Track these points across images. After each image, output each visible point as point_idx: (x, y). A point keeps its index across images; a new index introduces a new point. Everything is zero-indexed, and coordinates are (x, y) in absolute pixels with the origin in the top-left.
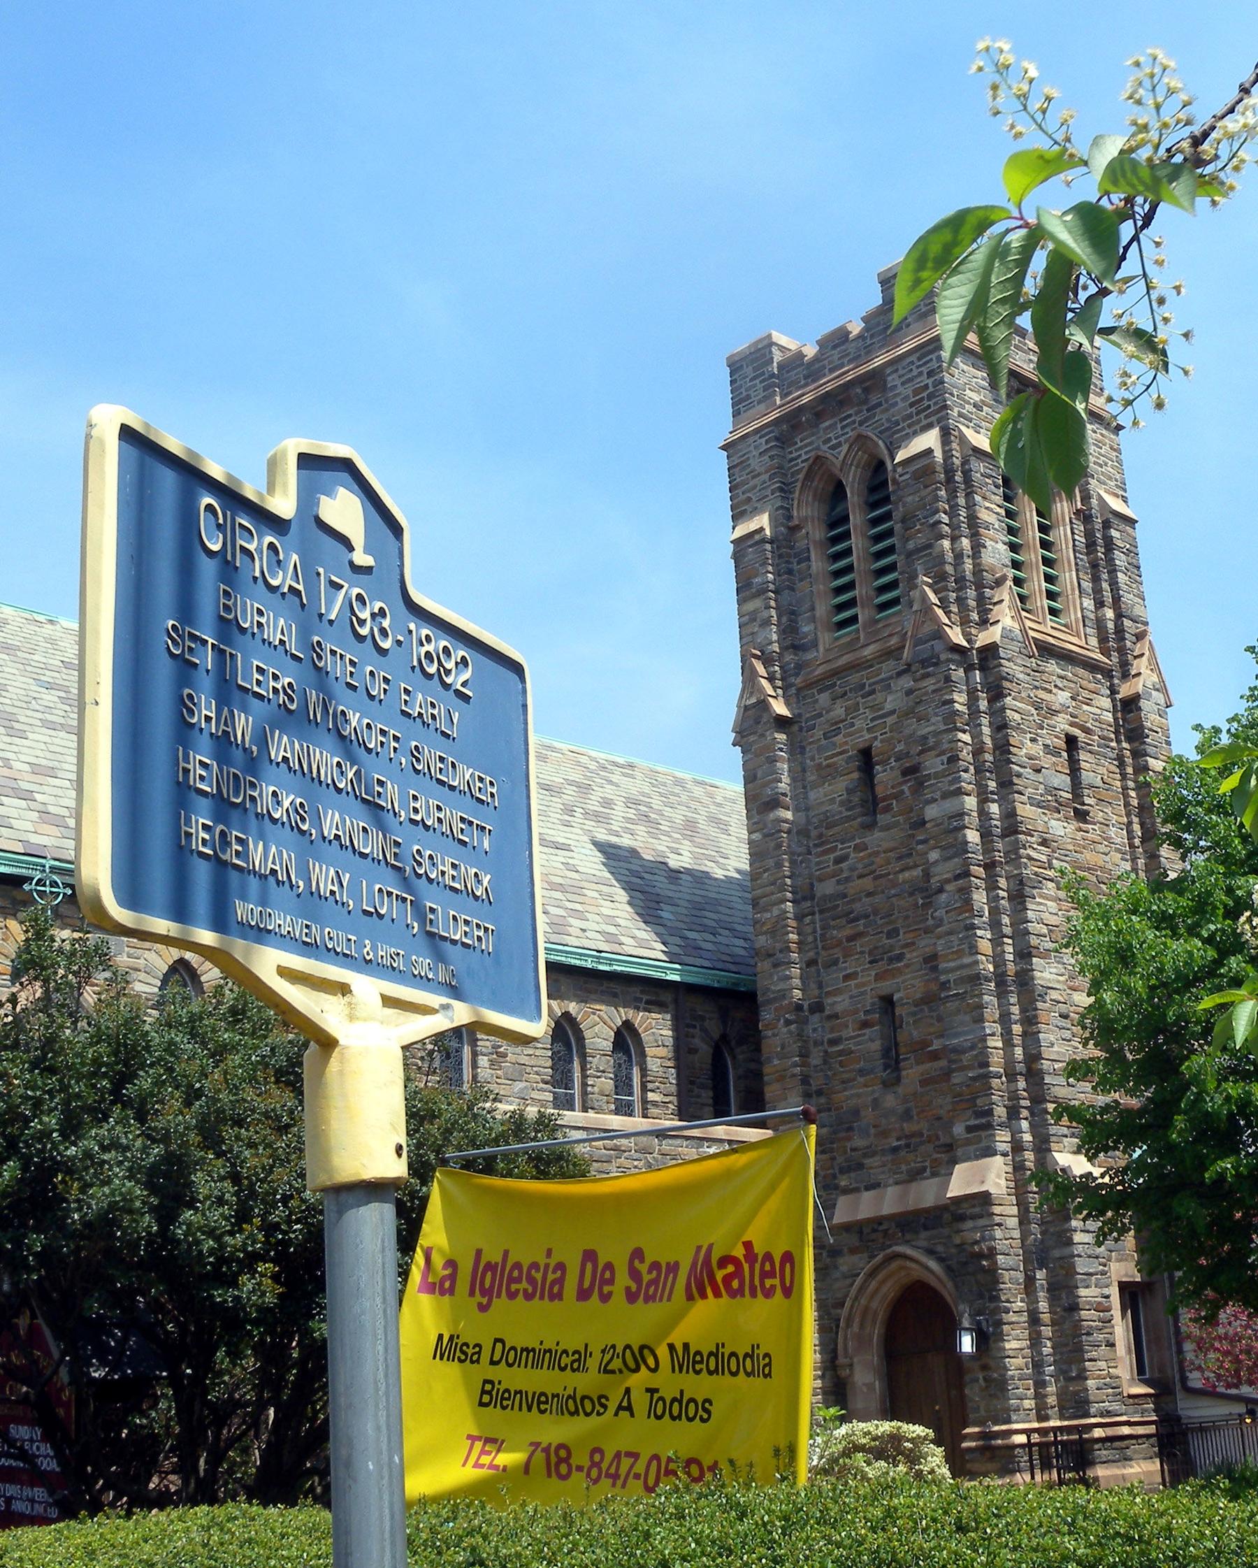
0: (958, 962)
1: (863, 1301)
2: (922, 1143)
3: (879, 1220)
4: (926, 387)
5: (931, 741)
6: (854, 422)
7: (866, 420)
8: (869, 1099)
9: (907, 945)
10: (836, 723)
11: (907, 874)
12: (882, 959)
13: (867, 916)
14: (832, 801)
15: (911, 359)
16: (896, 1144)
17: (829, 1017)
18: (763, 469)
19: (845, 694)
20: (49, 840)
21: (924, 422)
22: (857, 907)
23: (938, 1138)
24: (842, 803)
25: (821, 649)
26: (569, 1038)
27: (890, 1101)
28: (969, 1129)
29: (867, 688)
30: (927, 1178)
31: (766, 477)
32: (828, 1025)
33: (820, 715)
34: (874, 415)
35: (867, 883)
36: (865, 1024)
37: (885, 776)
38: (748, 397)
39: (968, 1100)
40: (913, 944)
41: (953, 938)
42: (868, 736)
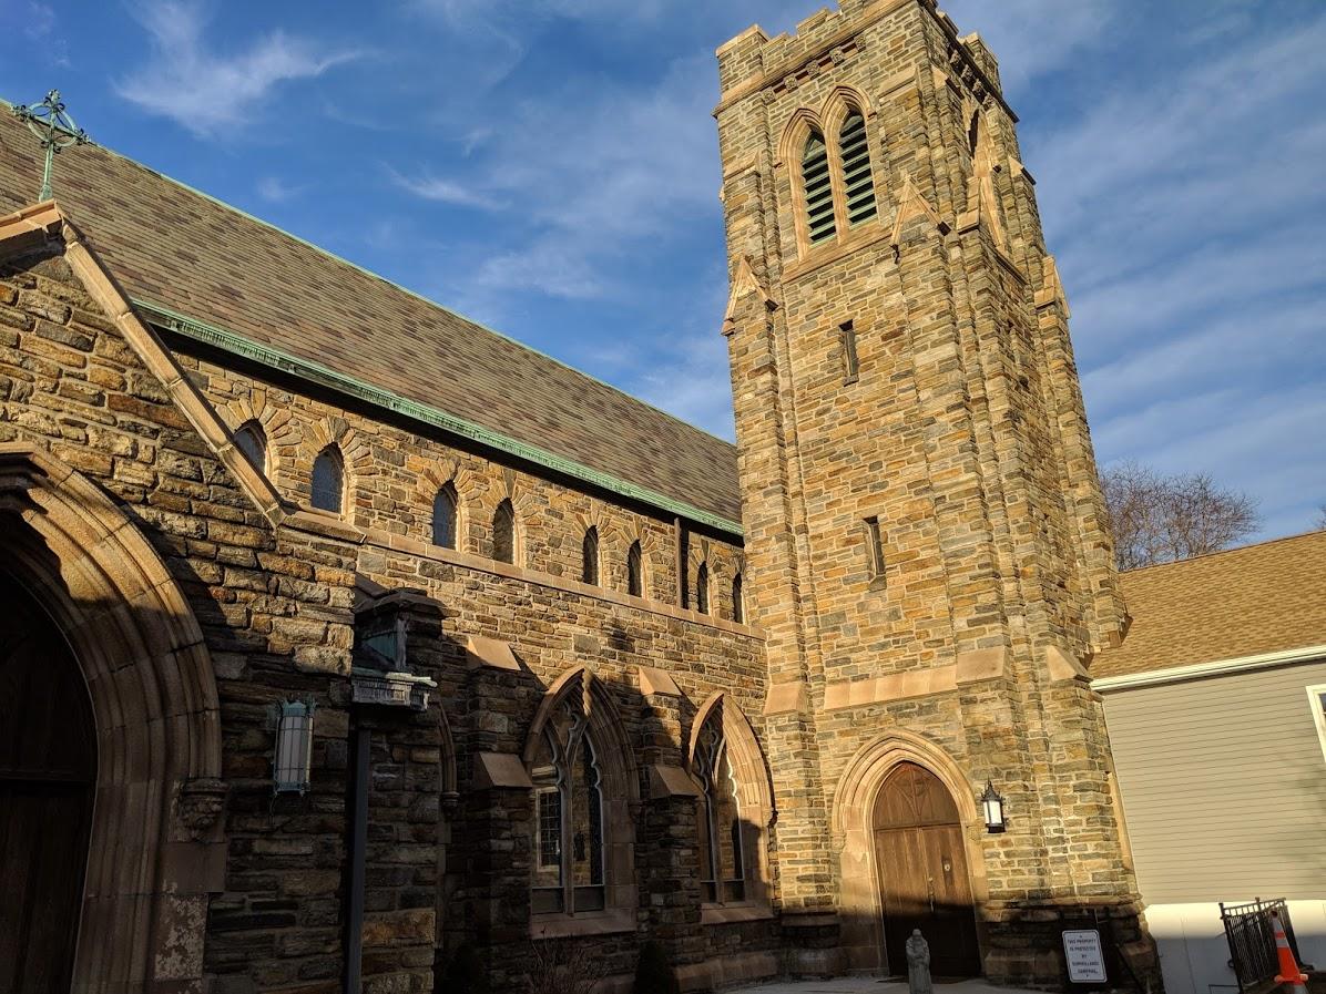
1: (855, 779)
3: (871, 706)
4: (904, 36)
6: (832, 80)
8: (855, 603)
10: (819, 306)
12: (866, 487)
13: (849, 454)
14: (815, 367)
15: (888, 18)
16: (883, 640)
17: (813, 538)
18: (750, 124)
19: (826, 283)
21: (902, 64)
22: (840, 449)
24: (823, 368)
27: (877, 604)
28: (971, 623)
29: (847, 276)
30: (917, 669)
31: (753, 130)
34: (851, 71)
35: (851, 428)
36: (849, 542)
37: (866, 344)
38: (736, 75)
40: (897, 473)
42: (848, 313)
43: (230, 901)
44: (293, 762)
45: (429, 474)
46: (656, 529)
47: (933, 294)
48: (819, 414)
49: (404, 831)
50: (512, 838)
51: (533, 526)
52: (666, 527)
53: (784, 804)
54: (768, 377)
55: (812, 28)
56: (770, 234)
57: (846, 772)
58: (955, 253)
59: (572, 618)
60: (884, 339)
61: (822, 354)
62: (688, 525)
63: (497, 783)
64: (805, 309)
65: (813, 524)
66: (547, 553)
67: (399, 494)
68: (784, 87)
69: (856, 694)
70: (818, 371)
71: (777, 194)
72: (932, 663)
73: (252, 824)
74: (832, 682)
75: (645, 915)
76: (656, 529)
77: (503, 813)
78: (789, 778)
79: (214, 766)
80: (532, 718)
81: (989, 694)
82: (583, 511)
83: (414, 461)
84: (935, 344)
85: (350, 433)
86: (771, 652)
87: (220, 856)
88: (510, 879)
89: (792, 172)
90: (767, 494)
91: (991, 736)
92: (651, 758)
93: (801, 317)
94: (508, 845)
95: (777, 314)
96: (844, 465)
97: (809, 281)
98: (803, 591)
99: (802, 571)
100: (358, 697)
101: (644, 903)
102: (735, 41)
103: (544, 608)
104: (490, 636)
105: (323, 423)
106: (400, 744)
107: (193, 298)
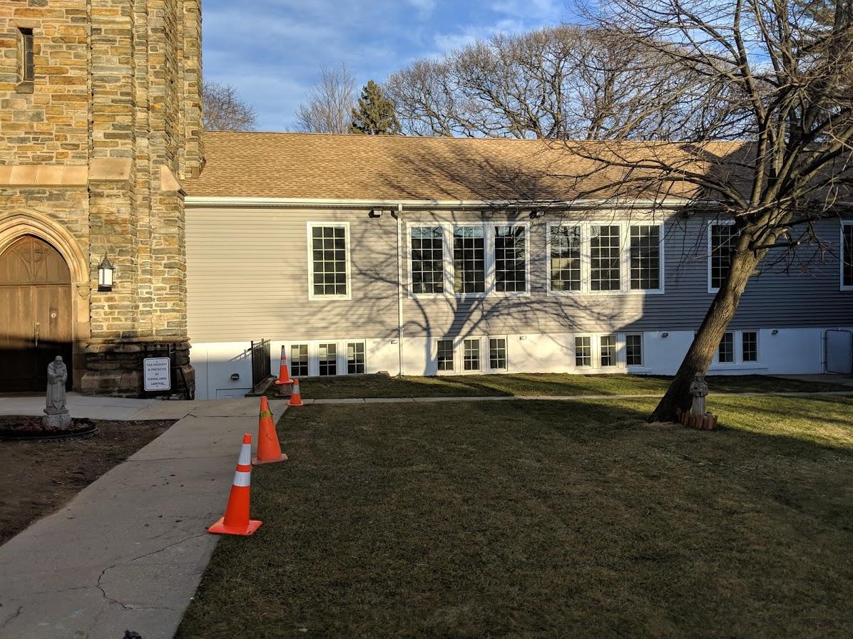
0: (112, 19)
2: (51, 139)
16: (23, 135)
20: (641, 299)
23: (66, 139)
26: (845, 273)
27: (21, 104)
28: (107, 136)
30: (53, 164)
39: (109, 116)
72: (67, 161)
81: (115, 192)
91: (111, 223)
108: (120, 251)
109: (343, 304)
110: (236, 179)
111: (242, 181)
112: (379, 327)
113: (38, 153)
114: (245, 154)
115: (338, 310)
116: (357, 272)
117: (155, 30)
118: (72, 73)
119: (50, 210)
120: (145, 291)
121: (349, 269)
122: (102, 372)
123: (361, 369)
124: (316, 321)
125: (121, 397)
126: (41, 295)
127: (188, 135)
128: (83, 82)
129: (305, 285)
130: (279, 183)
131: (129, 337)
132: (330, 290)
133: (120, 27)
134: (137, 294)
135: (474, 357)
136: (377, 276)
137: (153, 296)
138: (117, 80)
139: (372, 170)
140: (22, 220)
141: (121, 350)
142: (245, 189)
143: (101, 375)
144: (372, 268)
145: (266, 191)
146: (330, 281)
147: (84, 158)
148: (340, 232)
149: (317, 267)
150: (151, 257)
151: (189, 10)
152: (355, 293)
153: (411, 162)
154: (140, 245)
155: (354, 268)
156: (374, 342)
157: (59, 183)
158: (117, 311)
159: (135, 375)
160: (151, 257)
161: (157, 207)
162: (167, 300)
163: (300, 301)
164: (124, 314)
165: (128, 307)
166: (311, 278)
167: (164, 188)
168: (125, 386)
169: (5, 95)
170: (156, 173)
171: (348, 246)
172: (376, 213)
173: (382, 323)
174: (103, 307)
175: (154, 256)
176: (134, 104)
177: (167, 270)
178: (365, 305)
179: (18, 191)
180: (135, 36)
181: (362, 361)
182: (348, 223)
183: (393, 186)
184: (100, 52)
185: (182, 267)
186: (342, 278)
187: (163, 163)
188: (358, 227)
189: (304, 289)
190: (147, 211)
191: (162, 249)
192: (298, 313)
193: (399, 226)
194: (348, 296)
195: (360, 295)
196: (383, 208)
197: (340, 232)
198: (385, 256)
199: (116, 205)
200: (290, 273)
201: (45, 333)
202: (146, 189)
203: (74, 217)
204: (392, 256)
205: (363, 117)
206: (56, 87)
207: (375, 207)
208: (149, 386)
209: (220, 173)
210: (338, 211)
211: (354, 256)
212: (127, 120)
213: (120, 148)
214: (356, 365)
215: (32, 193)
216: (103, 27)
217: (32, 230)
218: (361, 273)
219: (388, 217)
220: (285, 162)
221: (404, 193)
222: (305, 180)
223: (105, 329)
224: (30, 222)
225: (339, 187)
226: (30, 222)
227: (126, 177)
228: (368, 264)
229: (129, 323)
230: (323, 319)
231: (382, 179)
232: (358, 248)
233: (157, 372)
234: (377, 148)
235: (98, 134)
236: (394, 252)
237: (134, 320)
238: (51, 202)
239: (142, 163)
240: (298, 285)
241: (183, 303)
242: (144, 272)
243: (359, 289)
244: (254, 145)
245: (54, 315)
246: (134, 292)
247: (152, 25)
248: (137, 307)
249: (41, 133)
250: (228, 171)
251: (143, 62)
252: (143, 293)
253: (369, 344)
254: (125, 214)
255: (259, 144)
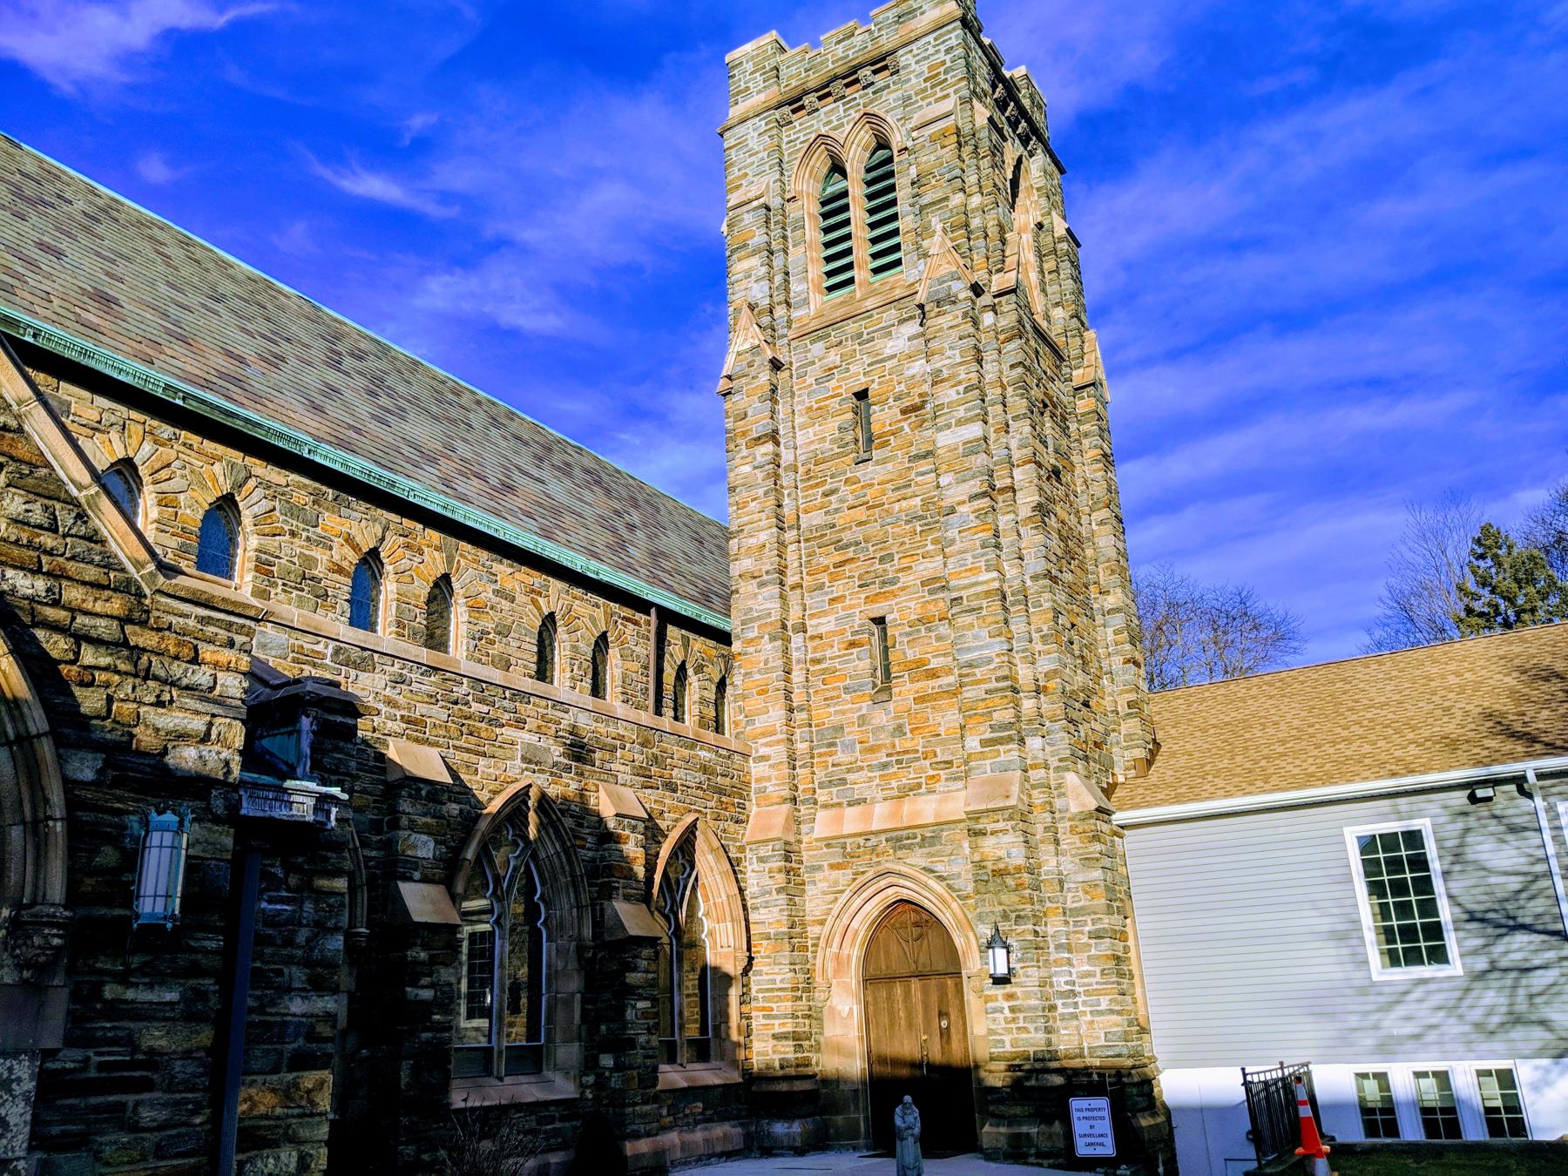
0: (973, 580)
2: (918, 759)
4: (944, 63)
5: (945, 374)
7: (872, 102)
9: (902, 570)
11: (904, 504)
13: (858, 544)
16: (885, 759)
17: (812, 638)
21: (939, 95)
22: (847, 537)
24: (833, 441)
25: (812, 306)
27: (881, 717)
28: (985, 743)
32: (810, 644)
33: (813, 363)
36: (852, 644)
37: (883, 417)
39: (983, 715)
41: (969, 556)
42: (863, 379)
43: (69, 1060)
44: (159, 885)
45: (349, 540)
46: (628, 620)
47: (961, 364)
48: (826, 495)
49: (298, 975)
50: (432, 986)
51: (476, 609)
52: (640, 617)
53: (762, 949)
54: (769, 447)
55: (839, 42)
56: (778, 279)
57: (835, 912)
58: (988, 319)
59: (520, 723)
60: (904, 412)
61: (832, 425)
62: (667, 617)
63: (416, 918)
64: (815, 372)
65: (815, 622)
66: (492, 643)
67: (310, 562)
68: (802, 107)
69: (852, 820)
70: (827, 445)
71: (789, 233)
72: (940, 787)
73: (103, 964)
74: (825, 806)
75: (591, 1079)
76: (628, 620)
77: (423, 955)
78: (770, 917)
79: (56, 888)
80: (464, 843)
81: (1001, 825)
82: (540, 594)
83: (331, 522)
84: (960, 423)
85: (252, 483)
86: (756, 770)
87: (58, 1005)
88: (426, 1035)
89: (808, 210)
90: (762, 585)
91: (1000, 873)
92: (607, 892)
93: (810, 380)
94: (427, 994)
95: (783, 375)
96: (851, 555)
97: (820, 338)
98: (797, 700)
99: (797, 676)
100: (248, 809)
101: (589, 1064)
102: (748, 48)
103: (485, 709)
104: (417, 740)
105: (217, 468)
106: (298, 869)
107: (56, 302)
108: (1018, 917)
109: (1445, 985)
110: (1208, 768)
111: (1219, 771)
112: (1538, 1033)
113: (904, 781)
114: (1227, 719)
115: (1437, 999)
116: (1465, 916)
117: (1035, 578)
118: (935, 663)
119: (924, 863)
120: (1062, 980)
121: (1445, 913)
122: (1012, 1121)
123: (1519, 1127)
124: (1393, 1023)
125: (1040, 1165)
126: (925, 992)
127: (1123, 709)
128: (950, 671)
129: (1360, 950)
130: (1283, 764)
131: (1043, 1060)
132: (1413, 957)
133: (986, 588)
134: (1052, 985)
135: (1508, 1110)
136: (1511, 923)
137: (1077, 988)
138: (990, 661)
139: (1468, 708)
140: (883, 883)
141: (1033, 1083)
142: (1221, 783)
143: (1009, 1125)
144: (1496, 906)
145: (1259, 784)
146: (1414, 939)
147: (960, 778)
148: (1414, 838)
149: (1384, 912)
150: (1067, 922)
151: (1101, 523)
152: (1469, 960)
153: (1558, 676)
154: (1048, 904)
155: (1457, 910)
156: (1537, 1068)
157: (931, 820)
158: (1021, 1016)
159: (1057, 1127)
160: (1067, 922)
161: (1069, 841)
162: (1098, 993)
163: (1356, 983)
164: (1032, 1021)
165: (1035, 1008)
166: (1370, 936)
167: (1074, 809)
168: (1045, 1146)
169: (860, 709)
170: (1060, 786)
171: (1435, 866)
172: (1480, 793)
173: (1543, 1023)
174: (1001, 1010)
175: (1071, 920)
176: (1015, 691)
177: (1093, 941)
178: (1495, 984)
179: (883, 837)
180: (1008, 594)
181: (1517, 1110)
182: (1427, 821)
183: (1512, 735)
184: (964, 628)
185: (1122, 936)
186: (1435, 931)
187: (1068, 770)
188: (1450, 827)
189: (1360, 958)
190: (1052, 847)
191: (1082, 908)
192: (1356, 1008)
193: (1543, 816)
194: (1456, 967)
195: (1481, 964)
196: (1495, 782)
197: (1414, 838)
198: (1521, 878)
199: (1005, 847)
200: (1326, 928)
201: (936, 1054)
202: (1047, 814)
203: (955, 870)
204: (1537, 878)
205: (1481, 591)
206: (918, 685)
207: (1477, 783)
208: (1082, 1150)
209: (1183, 761)
210: (1402, 801)
211: (1451, 884)
212: (1007, 715)
213: (1002, 758)
214: (1506, 1118)
215: (899, 839)
216: (964, 593)
217: (905, 894)
218: (1472, 917)
219: (1513, 799)
220: (1296, 723)
221: (1538, 746)
222: (1331, 751)
223: (1008, 1048)
224: (902, 882)
225: (1398, 753)
226: (902, 882)
227: (1012, 802)
228: (1484, 898)
229: (1041, 1036)
230: (1408, 1018)
231: (1490, 724)
232: (1457, 868)
233: (1092, 1122)
234: (1481, 663)
235: (973, 743)
236: (1540, 868)
237: (1048, 1030)
238: (925, 850)
239: (1036, 775)
240: (1344, 951)
241: (1128, 998)
242: (1058, 947)
243: (1475, 952)
244: (1243, 700)
245: (944, 1023)
246: (1044, 983)
247: (1030, 572)
248: (1053, 1008)
249: (905, 752)
250: (1197, 755)
251: (1023, 627)
252: (1060, 982)
253: (1525, 1073)
254: (1018, 857)
255: (1253, 697)
